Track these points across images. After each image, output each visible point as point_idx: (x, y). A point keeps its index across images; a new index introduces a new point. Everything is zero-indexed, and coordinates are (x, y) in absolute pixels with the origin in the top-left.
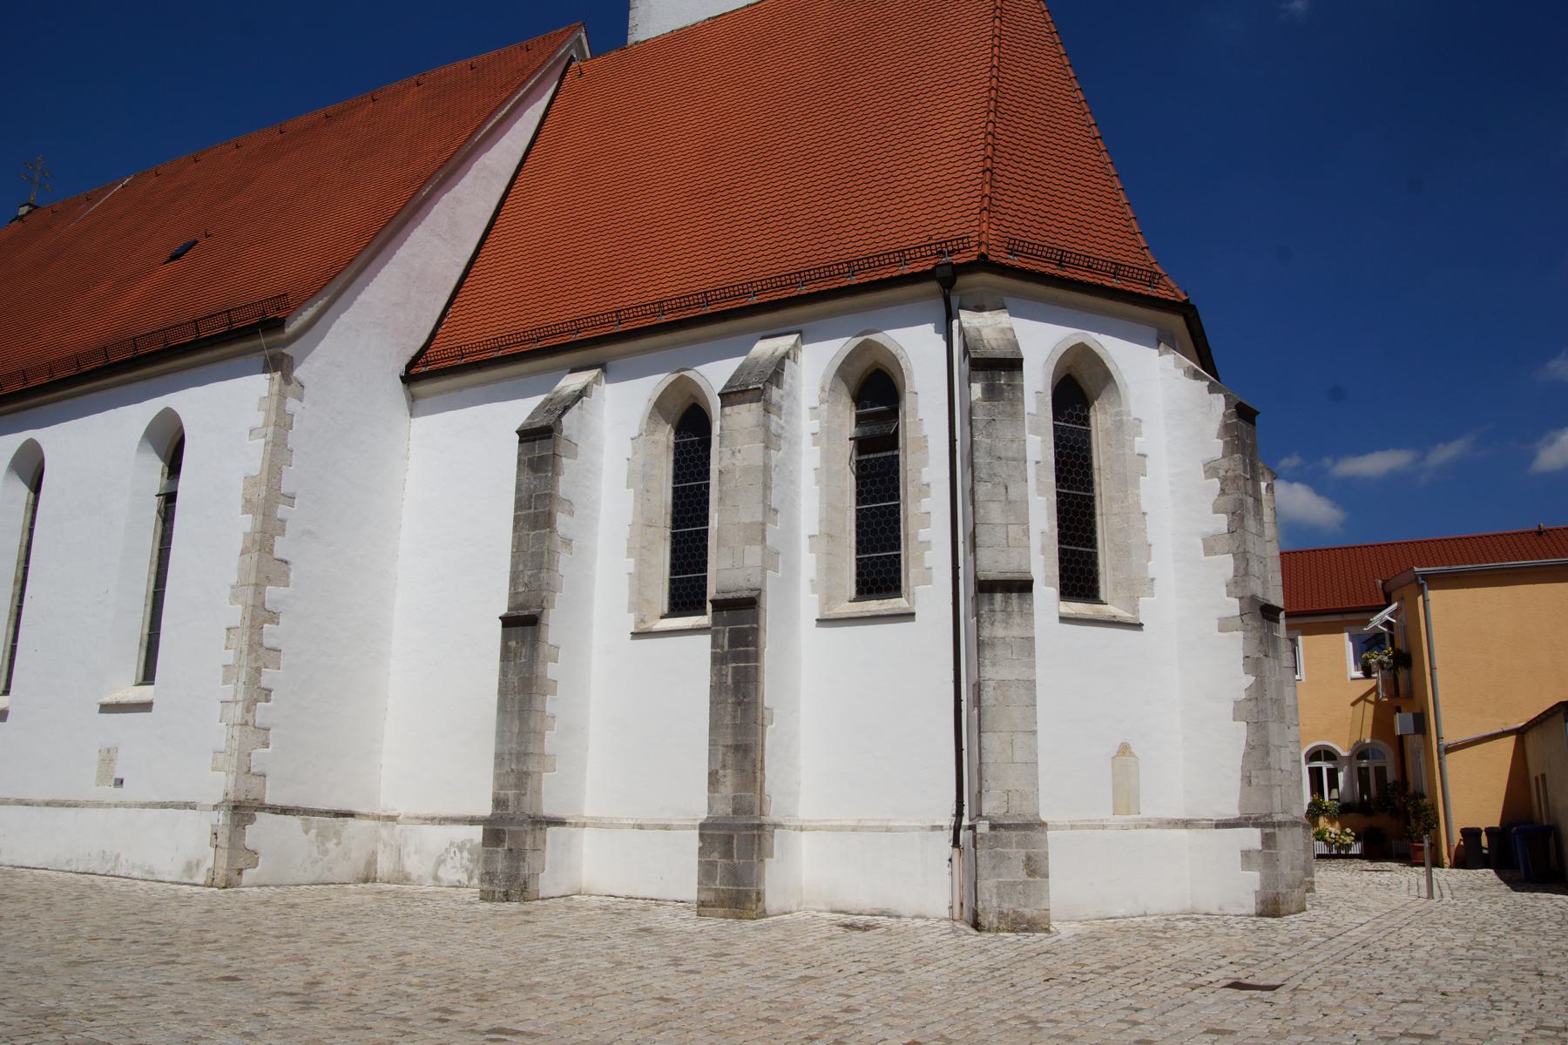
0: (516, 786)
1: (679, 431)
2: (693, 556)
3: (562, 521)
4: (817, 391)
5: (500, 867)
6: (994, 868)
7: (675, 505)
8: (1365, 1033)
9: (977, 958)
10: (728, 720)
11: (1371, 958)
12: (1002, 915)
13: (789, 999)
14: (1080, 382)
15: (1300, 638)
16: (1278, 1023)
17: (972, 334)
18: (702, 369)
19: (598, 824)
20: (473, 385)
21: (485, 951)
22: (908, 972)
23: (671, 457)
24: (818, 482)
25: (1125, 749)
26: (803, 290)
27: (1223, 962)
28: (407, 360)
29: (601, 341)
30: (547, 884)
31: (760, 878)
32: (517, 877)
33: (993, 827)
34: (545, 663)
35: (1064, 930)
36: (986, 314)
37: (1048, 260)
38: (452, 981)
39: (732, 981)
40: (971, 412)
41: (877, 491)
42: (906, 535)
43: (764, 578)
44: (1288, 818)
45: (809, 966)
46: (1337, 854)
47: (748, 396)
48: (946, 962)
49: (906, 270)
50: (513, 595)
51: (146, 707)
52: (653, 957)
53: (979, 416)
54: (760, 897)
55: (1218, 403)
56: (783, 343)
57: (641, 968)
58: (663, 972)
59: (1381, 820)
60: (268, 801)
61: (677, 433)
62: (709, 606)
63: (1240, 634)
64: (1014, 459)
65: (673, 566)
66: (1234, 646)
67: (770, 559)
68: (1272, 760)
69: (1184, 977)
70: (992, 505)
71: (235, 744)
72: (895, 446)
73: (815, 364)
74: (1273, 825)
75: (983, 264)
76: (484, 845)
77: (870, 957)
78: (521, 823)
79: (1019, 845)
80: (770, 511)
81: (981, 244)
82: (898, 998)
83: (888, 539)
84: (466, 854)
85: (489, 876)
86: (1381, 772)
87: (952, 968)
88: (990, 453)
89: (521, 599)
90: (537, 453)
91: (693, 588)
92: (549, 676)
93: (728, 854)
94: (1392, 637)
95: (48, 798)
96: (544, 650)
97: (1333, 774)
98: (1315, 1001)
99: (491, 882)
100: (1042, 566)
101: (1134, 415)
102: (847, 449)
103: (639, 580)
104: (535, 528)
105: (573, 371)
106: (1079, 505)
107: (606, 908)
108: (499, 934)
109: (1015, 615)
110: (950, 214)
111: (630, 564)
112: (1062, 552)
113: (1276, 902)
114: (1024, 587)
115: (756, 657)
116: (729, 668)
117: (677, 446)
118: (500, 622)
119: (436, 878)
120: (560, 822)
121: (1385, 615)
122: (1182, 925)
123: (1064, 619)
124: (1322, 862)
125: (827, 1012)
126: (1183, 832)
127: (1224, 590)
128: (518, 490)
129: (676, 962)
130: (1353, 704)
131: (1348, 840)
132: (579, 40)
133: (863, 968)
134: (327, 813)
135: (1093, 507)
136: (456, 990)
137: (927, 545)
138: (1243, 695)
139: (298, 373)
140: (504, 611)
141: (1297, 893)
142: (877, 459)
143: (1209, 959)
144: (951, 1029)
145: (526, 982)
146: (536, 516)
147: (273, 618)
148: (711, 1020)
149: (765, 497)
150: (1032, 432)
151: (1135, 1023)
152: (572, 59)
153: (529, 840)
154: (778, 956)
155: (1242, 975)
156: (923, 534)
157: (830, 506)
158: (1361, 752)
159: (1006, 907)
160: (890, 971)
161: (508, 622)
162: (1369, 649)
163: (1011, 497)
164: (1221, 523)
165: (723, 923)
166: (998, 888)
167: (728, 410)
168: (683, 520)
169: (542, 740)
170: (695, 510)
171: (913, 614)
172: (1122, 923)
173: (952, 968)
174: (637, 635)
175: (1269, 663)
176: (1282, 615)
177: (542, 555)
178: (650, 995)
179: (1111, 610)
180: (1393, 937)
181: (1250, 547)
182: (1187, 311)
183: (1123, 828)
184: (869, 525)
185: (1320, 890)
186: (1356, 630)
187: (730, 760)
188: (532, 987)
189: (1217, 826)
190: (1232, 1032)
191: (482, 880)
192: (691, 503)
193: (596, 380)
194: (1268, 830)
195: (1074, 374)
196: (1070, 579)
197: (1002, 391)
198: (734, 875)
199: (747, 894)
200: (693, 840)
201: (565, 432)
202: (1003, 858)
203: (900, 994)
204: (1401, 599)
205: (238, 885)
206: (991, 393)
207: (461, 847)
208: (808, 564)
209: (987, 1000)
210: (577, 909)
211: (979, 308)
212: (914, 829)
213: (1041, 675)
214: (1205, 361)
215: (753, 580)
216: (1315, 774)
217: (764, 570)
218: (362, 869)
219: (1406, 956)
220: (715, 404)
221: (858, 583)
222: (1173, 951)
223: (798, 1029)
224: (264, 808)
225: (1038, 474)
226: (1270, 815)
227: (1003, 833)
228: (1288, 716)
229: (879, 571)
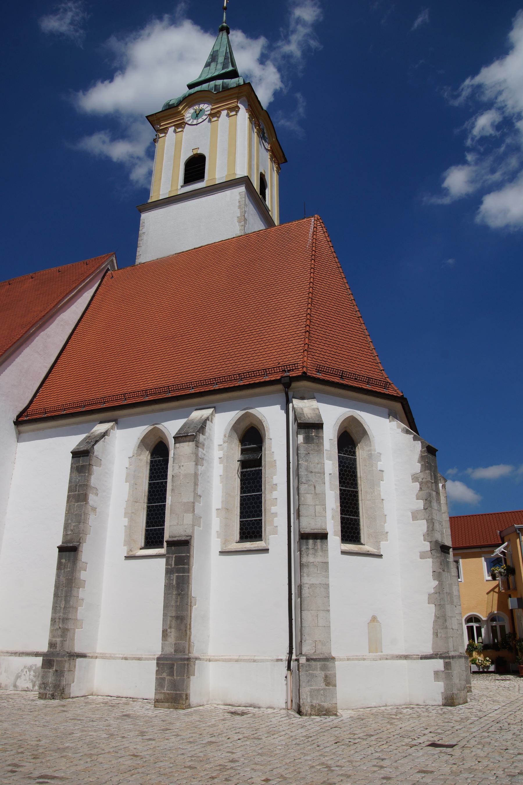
0: (62, 636)
1: (152, 454)
2: (158, 518)
3: (92, 499)
4: (222, 437)
5: (50, 680)
6: (308, 682)
7: (149, 492)
8: (500, 772)
9: (300, 731)
10: (173, 603)
11: (501, 729)
12: (313, 707)
13: (201, 754)
14: (351, 434)
15: (460, 560)
16: (455, 766)
17: (298, 411)
18: (166, 424)
19: (104, 657)
21: (39, 728)
22: (264, 739)
23: (149, 468)
24: (221, 482)
25: (374, 619)
26: (217, 387)
27: (426, 732)
28: (17, 413)
29: (116, 409)
30: (75, 690)
31: (188, 687)
32: (59, 686)
33: (308, 660)
34: (80, 571)
35: (345, 714)
36: (305, 401)
37: (335, 375)
38: (20, 747)
39: (172, 745)
40: (298, 449)
41: (251, 487)
42: (265, 510)
43: (193, 530)
44: (457, 654)
45: (212, 735)
46: (483, 671)
47: (188, 438)
48: (283, 733)
49: (267, 379)
50: (65, 535)
52: (130, 731)
53: (302, 451)
54: (187, 697)
55: (418, 445)
56: (206, 413)
57: (123, 737)
58: (135, 740)
59: (504, 653)
61: (152, 455)
62: (165, 544)
63: (430, 560)
64: (319, 473)
65: (147, 523)
66: (428, 565)
67: (197, 521)
68: (448, 624)
69: (407, 740)
70: (308, 496)
72: (260, 465)
73: (221, 424)
74: (449, 657)
75: (304, 377)
77: (244, 730)
78: (63, 656)
80: (197, 496)
81: (303, 367)
82: (259, 754)
83: (256, 487)
84: (32, 673)
85: (44, 685)
86: (502, 628)
87: (287, 736)
88: (307, 469)
89: (69, 537)
90: (81, 463)
91: (157, 534)
93: (171, 674)
94: (505, 559)
96: (80, 564)
97: (479, 629)
98: (473, 753)
99: (45, 688)
100: (332, 525)
101: (377, 451)
102: (236, 466)
103: (130, 530)
104: (78, 501)
105: (101, 422)
106: (351, 495)
107: (106, 703)
108: (48, 718)
109: (319, 550)
110: (287, 350)
111: (125, 521)
112: (342, 519)
113: (452, 698)
114: (323, 536)
115: (188, 571)
117: (151, 462)
118: (57, 549)
119: (15, 686)
120: (83, 656)
121: (501, 548)
122: (405, 711)
123: (343, 553)
124: (476, 676)
125: (221, 762)
126: (405, 661)
127: (422, 538)
128: (70, 481)
129: (142, 733)
130: (488, 593)
131: (488, 664)
132: (112, 261)
133: (241, 736)
135: (358, 496)
136: (22, 753)
137: (275, 515)
138: (432, 591)
140: (60, 543)
141: (462, 693)
142: (251, 471)
143: (419, 730)
144: (286, 771)
145: (61, 746)
148: (160, 768)
149: (195, 489)
150: (328, 459)
151: (382, 767)
152: (108, 270)
153: (67, 665)
154: (196, 730)
155: (436, 739)
156: (273, 509)
157: (227, 495)
158: (492, 618)
159: (315, 702)
160: (255, 738)
161: (61, 549)
162: (494, 565)
163: (317, 492)
164: (420, 504)
165: (168, 711)
166: (310, 692)
167: (177, 445)
168: (155, 477)
170: (159, 495)
171: (268, 550)
172: (374, 710)
173: (287, 736)
174: (127, 558)
175: (445, 575)
176: (451, 550)
177: (81, 516)
178: (128, 753)
179: (366, 548)
180: (512, 717)
181: (435, 517)
182: (402, 400)
183: (374, 660)
184: (247, 504)
185: (475, 691)
186: (488, 556)
187: (174, 624)
188: (65, 749)
189: (422, 658)
190: (432, 772)
191: (40, 688)
192: (158, 491)
193: (112, 428)
194: (447, 660)
195: (348, 431)
196: (346, 532)
197: (313, 439)
198: (175, 685)
199: (181, 695)
201: (95, 454)
202: (313, 676)
203: (260, 751)
204: (509, 541)
206: (308, 440)
207: (30, 669)
208: (215, 523)
209: (305, 755)
210: (90, 704)
211: (302, 398)
212: (267, 660)
213: (333, 581)
214: (412, 425)
215: (188, 531)
216: (470, 629)
217: (193, 526)
219: (519, 727)
220: (171, 442)
221: (240, 533)
222: (400, 726)
223: (206, 773)
225: (330, 480)
226: (448, 652)
227: (313, 663)
228: (455, 600)
229: (251, 528)
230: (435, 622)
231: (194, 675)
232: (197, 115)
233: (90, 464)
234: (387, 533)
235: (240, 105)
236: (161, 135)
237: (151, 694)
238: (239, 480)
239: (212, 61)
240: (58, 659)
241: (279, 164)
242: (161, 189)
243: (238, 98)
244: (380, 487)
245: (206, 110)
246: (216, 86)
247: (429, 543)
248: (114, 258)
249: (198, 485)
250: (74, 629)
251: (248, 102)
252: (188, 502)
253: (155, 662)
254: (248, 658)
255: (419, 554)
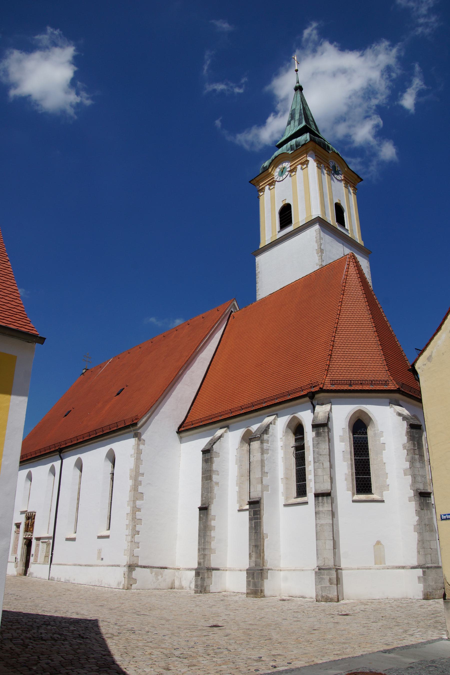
4: (282, 433)
6: (320, 582)
10: (253, 538)
12: (322, 597)
19: (231, 570)
20: (196, 433)
25: (378, 543)
28: (178, 426)
29: (226, 419)
30: (213, 588)
34: (211, 521)
36: (324, 406)
47: (256, 439)
50: (202, 501)
51: (108, 537)
60: (139, 564)
63: (414, 503)
70: (319, 469)
71: (129, 548)
76: (195, 576)
79: (327, 575)
85: (196, 586)
89: (204, 502)
92: (212, 525)
93: (253, 578)
95: (86, 564)
96: (210, 517)
99: (197, 588)
101: (380, 430)
104: (207, 480)
109: (325, 503)
111: (237, 489)
115: (260, 518)
116: (253, 522)
119: (190, 588)
120: (272, 569)
123: (354, 501)
127: (409, 487)
128: (202, 469)
132: (234, 304)
134: (158, 568)
138: (416, 523)
139: (143, 437)
140: (199, 505)
146: (207, 476)
147: (139, 510)
153: (206, 575)
157: (287, 469)
159: (324, 594)
161: (201, 509)
163: (324, 467)
164: (407, 465)
166: (321, 588)
169: (210, 544)
171: (308, 502)
174: (239, 511)
179: (375, 496)
183: (378, 569)
193: (226, 432)
194: (424, 570)
197: (321, 433)
198: (255, 585)
200: (245, 574)
205: (131, 589)
208: (281, 487)
211: (322, 404)
218: (170, 585)
224: (138, 566)
227: (322, 571)
230: (418, 544)
231: (267, 579)
232: (282, 172)
233: (211, 458)
234: (388, 485)
235: (309, 158)
236: (261, 194)
237: (244, 590)
238: (294, 459)
239: (291, 120)
240: (203, 571)
241: (354, 187)
242: (267, 237)
243: (307, 153)
244: (382, 455)
245: (287, 167)
246: (291, 146)
247: (413, 491)
248: (235, 302)
249: (264, 466)
250: (210, 555)
251: (315, 153)
252: (259, 478)
253: (246, 572)
254: (300, 568)
255: (408, 498)
